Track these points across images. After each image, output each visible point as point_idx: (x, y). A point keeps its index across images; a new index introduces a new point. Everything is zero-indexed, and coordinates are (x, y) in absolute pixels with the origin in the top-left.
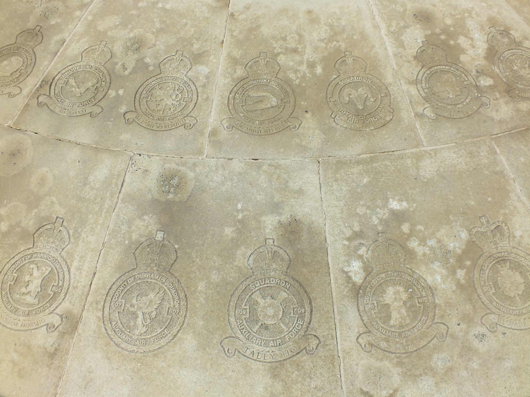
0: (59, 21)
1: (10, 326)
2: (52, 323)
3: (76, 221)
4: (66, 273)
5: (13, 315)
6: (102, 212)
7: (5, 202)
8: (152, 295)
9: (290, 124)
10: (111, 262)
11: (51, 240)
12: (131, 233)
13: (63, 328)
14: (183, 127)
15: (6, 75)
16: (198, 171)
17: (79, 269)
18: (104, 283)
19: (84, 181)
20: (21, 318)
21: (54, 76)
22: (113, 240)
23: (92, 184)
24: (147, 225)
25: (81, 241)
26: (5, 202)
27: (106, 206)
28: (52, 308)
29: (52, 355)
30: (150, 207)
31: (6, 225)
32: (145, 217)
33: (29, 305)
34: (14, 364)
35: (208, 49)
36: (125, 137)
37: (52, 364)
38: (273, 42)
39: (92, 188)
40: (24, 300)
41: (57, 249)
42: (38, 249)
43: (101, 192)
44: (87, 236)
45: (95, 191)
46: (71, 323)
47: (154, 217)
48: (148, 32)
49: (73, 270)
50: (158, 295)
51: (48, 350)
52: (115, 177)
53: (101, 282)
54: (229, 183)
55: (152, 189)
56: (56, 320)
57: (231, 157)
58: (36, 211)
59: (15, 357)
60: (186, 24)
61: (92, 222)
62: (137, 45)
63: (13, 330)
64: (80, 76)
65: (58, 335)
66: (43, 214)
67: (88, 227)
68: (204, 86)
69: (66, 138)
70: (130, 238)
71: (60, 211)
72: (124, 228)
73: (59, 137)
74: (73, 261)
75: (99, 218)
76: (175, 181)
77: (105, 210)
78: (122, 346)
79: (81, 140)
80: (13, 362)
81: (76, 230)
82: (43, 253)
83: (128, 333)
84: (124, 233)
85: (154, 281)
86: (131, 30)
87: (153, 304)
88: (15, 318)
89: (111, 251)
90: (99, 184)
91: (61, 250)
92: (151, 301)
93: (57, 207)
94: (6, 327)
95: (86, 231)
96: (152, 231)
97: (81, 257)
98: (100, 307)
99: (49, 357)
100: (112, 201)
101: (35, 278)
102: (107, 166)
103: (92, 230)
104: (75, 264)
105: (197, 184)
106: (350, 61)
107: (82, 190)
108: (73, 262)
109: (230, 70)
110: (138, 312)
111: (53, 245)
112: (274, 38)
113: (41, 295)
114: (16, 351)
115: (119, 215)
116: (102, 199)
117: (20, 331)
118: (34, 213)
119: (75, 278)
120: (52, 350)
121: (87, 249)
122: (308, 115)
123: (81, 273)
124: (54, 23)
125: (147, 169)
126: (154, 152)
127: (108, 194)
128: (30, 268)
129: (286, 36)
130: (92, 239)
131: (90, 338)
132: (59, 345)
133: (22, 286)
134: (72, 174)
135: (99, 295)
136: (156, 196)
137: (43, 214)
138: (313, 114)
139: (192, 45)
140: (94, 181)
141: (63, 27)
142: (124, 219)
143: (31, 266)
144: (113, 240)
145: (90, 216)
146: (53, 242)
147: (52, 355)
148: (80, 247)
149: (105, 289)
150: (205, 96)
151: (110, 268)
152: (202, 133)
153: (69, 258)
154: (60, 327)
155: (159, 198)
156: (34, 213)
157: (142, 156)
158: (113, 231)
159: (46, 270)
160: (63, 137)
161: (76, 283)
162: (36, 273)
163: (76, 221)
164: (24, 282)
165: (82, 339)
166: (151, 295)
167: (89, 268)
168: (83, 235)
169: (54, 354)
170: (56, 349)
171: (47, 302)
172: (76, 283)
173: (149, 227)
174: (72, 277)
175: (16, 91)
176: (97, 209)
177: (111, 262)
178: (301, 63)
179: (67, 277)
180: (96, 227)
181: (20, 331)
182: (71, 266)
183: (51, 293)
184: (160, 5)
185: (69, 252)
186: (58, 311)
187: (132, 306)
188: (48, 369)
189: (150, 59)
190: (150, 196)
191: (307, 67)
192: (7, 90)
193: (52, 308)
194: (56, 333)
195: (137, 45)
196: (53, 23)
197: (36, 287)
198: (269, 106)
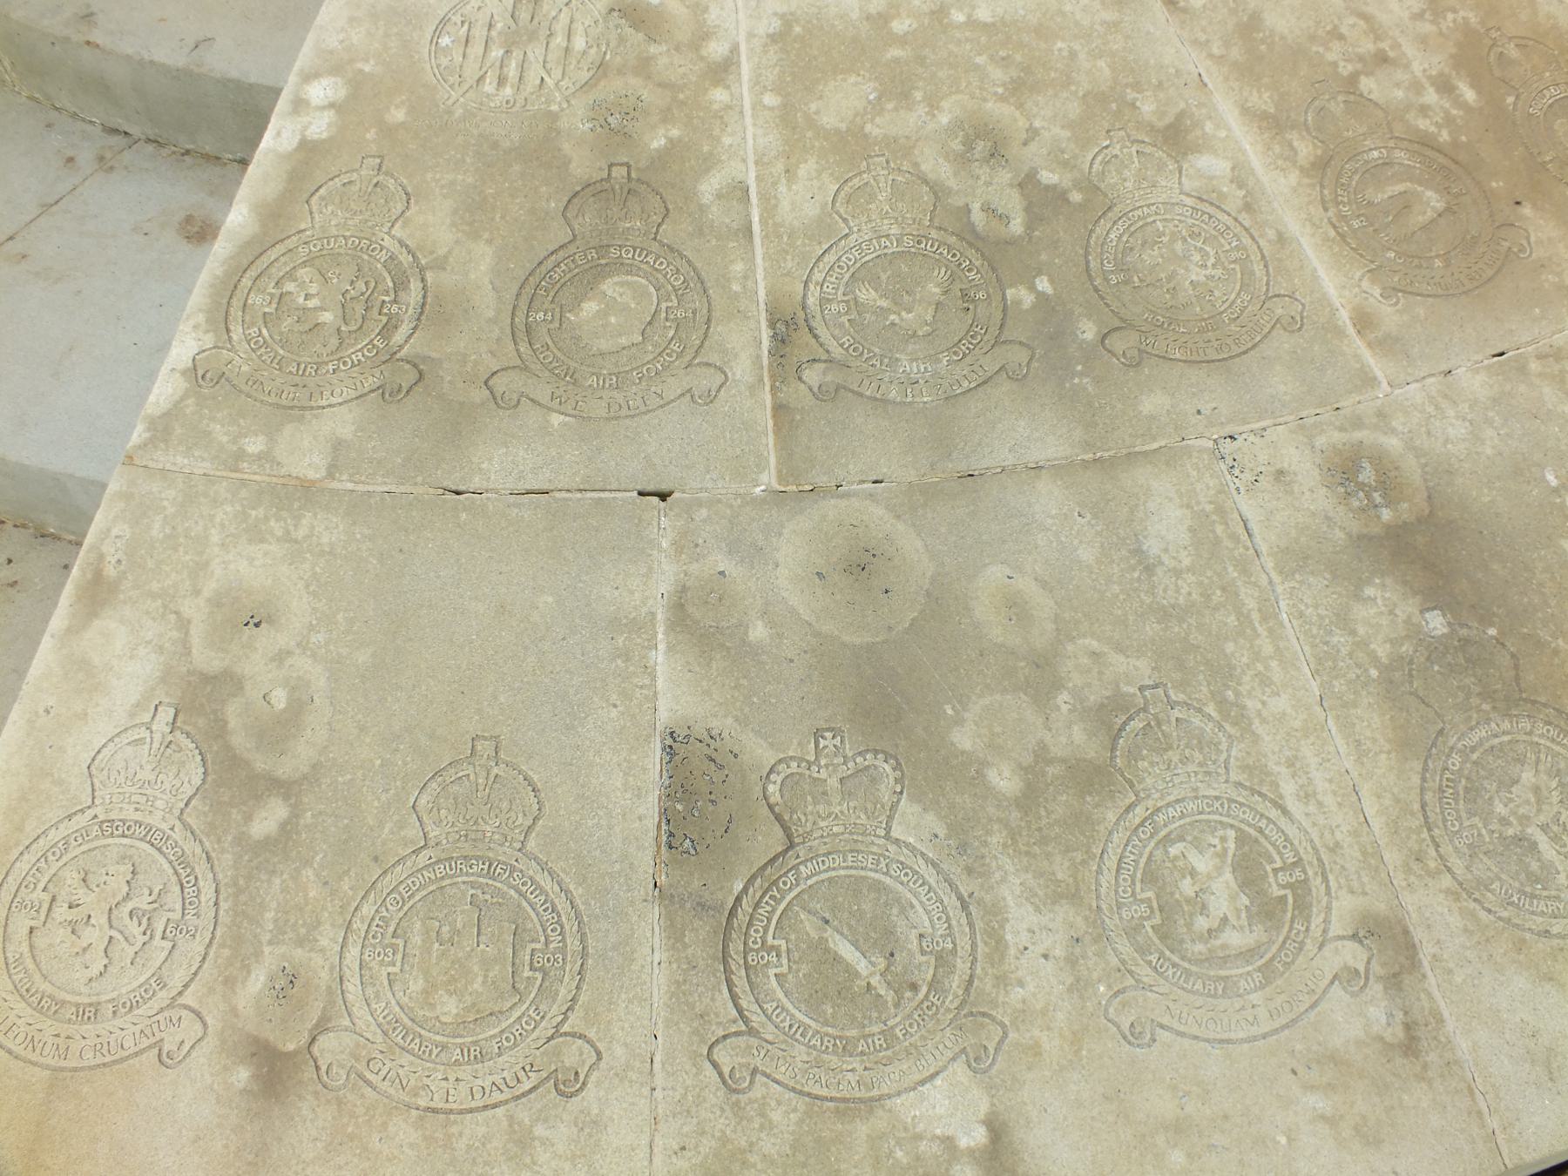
0: (675, 132)
1: (1241, 1035)
2: (1346, 968)
3: (1201, 677)
4: (1283, 822)
5: (1223, 1003)
6: (1251, 622)
7: (950, 712)
8: (1527, 776)
9: (1506, 244)
10: (1374, 740)
11: (1174, 756)
12: (1367, 645)
13: (1384, 965)
14: (1278, 330)
15: (623, 341)
16: (1400, 428)
17: (1307, 795)
18: (1398, 801)
19: (1140, 563)
20: (1255, 998)
21: (799, 298)
22: (1335, 683)
23: (1165, 559)
24: (1386, 612)
25: (1256, 722)
26: (950, 712)
27: (1251, 604)
28: (1316, 931)
29: (1410, 1046)
30: (1360, 561)
31: (1007, 774)
32: (1369, 591)
33: (1248, 954)
34: (1331, 1121)
35: (1182, 105)
36: (1153, 403)
37: (1425, 1067)
38: (1321, 50)
39: (1178, 573)
40: (1224, 947)
41: (1208, 773)
42: (1156, 796)
43: (1209, 573)
44: (1264, 703)
45: (1191, 578)
46: (1392, 946)
47: (1388, 581)
48: (985, 100)
49: (1292, 804)
50: (1541, 767)
51: (1389, 1039)
52: (1214, 517)
53: (1387, 802)
54: (1490, 432)
55: (1331, 514)
56: (1352, 955)
57: (1445, 368)
58: (1063, 697)
59: (1317, 1102)
60: (1073, 55)
61: (1245, 660)
62: (983, 143)
63: (1255, 1039)
64: (884, 277)
65: (1386, 988)
66: (1092, 698)
67: (1246, 679)
68: (1248, 207)
69: (985, 463)
70: (1375, 659)
71: (1136, 668)
72: (1338, 638)
73: (963, 467)
74: (1275, 785)
75: (1257, 642)
76: (1367, 475)
77: (1255, 616)
78: (1555, 930)
79: (1036, 455)
80: (1323, 1117)
81: (1222, 703)
82: (1178, 801)
83: (1545, 893)
84: (1350, 655)
85: (1506, 738)
86: (933, 105)
87: (1545, 793)
88: (1237, 1006)
89: (1353, 711)
90: (1184, 553)
91: (1222, 771)
92: (1537, 790)
93: (1119, 663)
94: (1228, 1041)
95: (1249, 693)
96: (1409, 617)
97: (1290, 763)
98: (1432, 864)
99: (1406, 1055)
100: (1255, 584)
101: (1209, 877)
102: (1171, 500)
103: (1265, 681)
104: (1288, 788)
105: (1423, 461)
106: (1513, 52)
107: (1154, 587)
108: (1278, 786)
109: (1277, 149)
110: (1529, 831)
111: (1191, 768)
112: (1313, 38)
113: (1267, 911)
114: (1309, 1088)
115: (1301, 615)
116: (1224, 589)
117: (1276, 1032)
118: (1065, 708)
119: (1314, 824)
120: (1401, 1034)
121: (1288, 734)
122: (1527, 210)
123: (1320, 804)
124: (663, 142)
125: (1278, 467)
126: (1260, 419)
127: (1231, 569)
128: (1176, 858)
129: (1335, 27)
130: (1281, 704)
131: (1468, 953)
132: (1406, 1013)
133: (1191, 915)
134: (1087, 554)
135: (1408, 838)
136: (1355, 527)
137: (1092, 698)
138: (1534, 206)
139: (1133, 105)
140: (1166, 550)
141: (706, 149)
142: (1321, 617)
143: (1174, 851)
144: (1335, 683)
145: (1230, 647)
146: (1185, 760)
147: (1410, 1046)
148: (1267, 738)
149: (1412, 814)
150: (1271, 234)
151: (1384, 756)
152: (1340, 332)
153: (1261, 782)
154: (1376, 967)
155: (1365, 531)
156: (1065, 708)
157: (1240, 439)
158: (1319, 661)
159: (1223, 839)
160: (976, 465)
161: (1327, 835)
162: (1202, 863)
163: (1201, 677)
164: (1188, 901)
165: (1451, 965)
166: (1524, 775)
167: (1330, 781)
168: (1251, 705)
169: (1413, 1041)
170: (1407, 1027)
171: (1292, 921)
172: (1327, 835)
173: (1397, 612)
174: (1306, 824)
175: (705, 380)
176: (1232, 620)
177: (1374, 740)
178: (1416, 87)
179: (1292, 831)
180: (1267, 668)
181: (1276, 1032)
182: (1281, 797)
183: (1282, 892)
184: (959, 17)
185: (1248, 766)
186: (1336, 929)
187: (1504, 821)
188: (1424, 1085)
189: (1052, 171)
190: (1340, 535)
191: (1438, 91)
192: (673, 387)
193: (1316, 931)
194: (1376, 988)
195: (983, 143)
196: (658, 143)
197: (1233, 898)
198: (1430, 214)
